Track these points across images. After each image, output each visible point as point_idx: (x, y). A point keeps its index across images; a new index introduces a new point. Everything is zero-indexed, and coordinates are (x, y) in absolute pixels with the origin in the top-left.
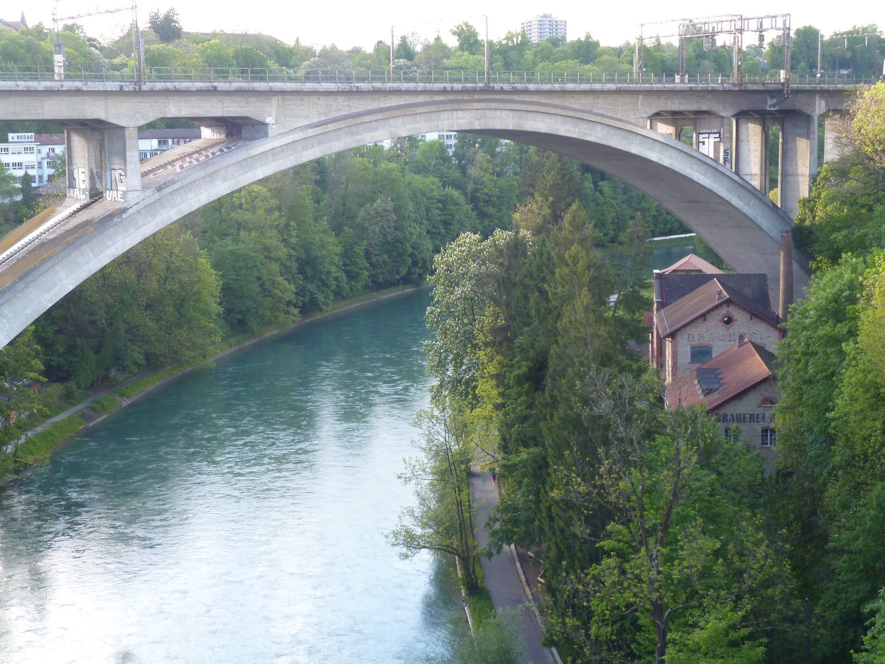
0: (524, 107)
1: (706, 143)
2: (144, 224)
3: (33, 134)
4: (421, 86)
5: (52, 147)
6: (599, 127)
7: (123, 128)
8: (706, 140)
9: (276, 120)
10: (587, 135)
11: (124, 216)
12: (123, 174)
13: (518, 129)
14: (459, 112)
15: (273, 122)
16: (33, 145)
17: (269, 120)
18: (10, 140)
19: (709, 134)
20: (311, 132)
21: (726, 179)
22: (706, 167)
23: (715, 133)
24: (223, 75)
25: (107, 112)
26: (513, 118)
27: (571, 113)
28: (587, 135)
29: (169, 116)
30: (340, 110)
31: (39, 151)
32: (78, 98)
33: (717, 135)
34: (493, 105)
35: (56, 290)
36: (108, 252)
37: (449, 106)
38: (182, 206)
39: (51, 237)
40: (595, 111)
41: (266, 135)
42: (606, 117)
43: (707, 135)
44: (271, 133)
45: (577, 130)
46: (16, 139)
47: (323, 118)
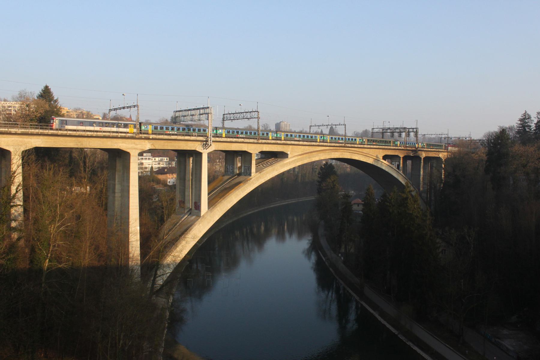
0: (353, 152)
1: (395, 165)
2: (255, 183)
3: (150, 154)
4: (329, 144)
5: (155, 158)
6: (371, 158)
7: (251, 154)
8: (395, 164)
9: (291, 153)
10: (368, 161)
11: (251, 180)
12: (249, 167)
13: (350, 158)
14: (336, 152)
15: (290, 153)
16: (151, 157)
17: (289, 153)
18: (144, 155)
19: (396, 162)
20: (299, 157)
21: (401, 176)
22: (396, 172)
23: (398, 162)
24: (15, 125)
25: (248, 149)
26: (350, 155)
27: (364, 154)
28: (368, 161)
29: (263, 150)
30: (307, 150)
31: (152, 159)
32: (8, 136)
33: (398, 162)
34: (345, 151)
35: (232, 203)
36: (246, 191)
37: (334, 151)
38: (265, 178)
39: (228, 186)
40: (370, 154)
41: (287, 157)
42: (372, 156)
43: (395, 162)
44: (289, 157)
45: (365, 159)
46: (145, 155)
47: (302, 153)
